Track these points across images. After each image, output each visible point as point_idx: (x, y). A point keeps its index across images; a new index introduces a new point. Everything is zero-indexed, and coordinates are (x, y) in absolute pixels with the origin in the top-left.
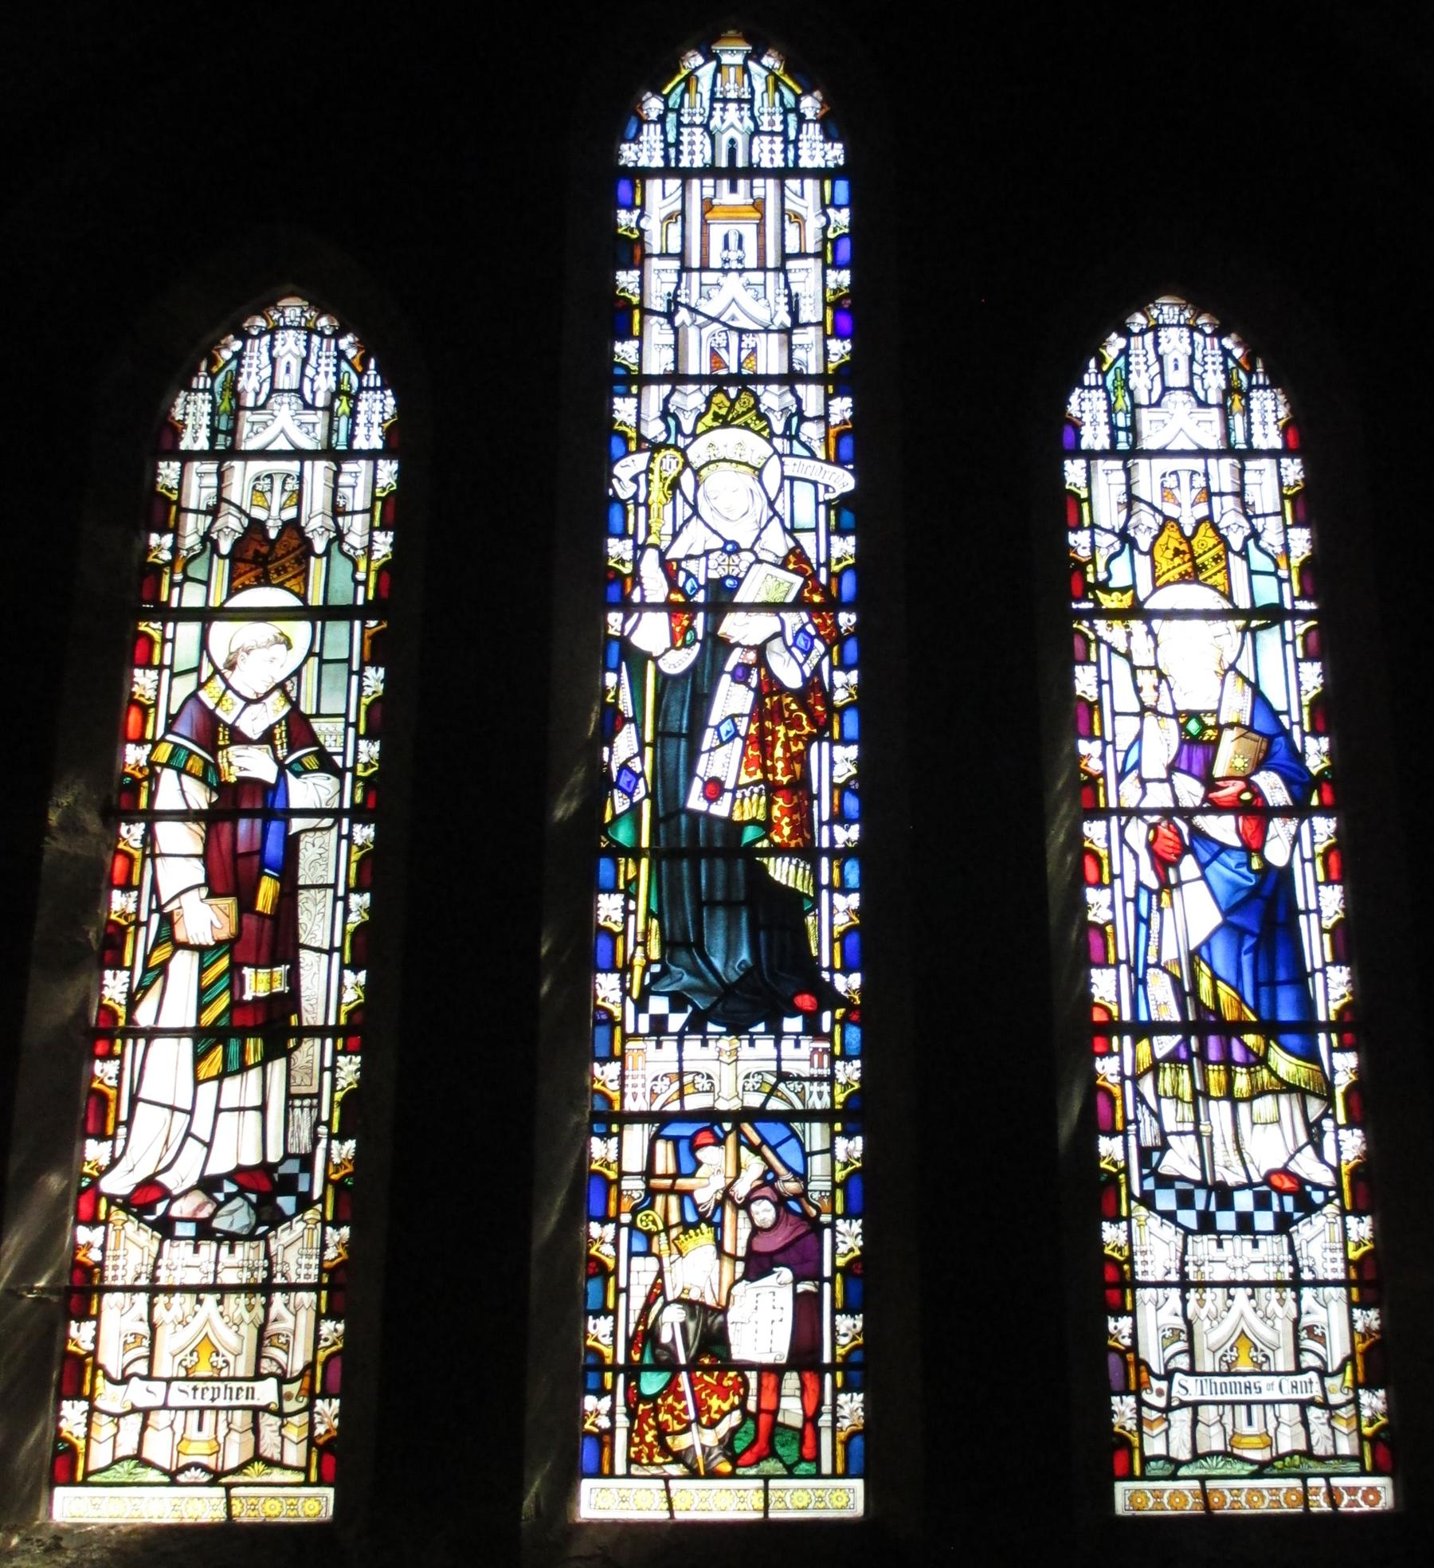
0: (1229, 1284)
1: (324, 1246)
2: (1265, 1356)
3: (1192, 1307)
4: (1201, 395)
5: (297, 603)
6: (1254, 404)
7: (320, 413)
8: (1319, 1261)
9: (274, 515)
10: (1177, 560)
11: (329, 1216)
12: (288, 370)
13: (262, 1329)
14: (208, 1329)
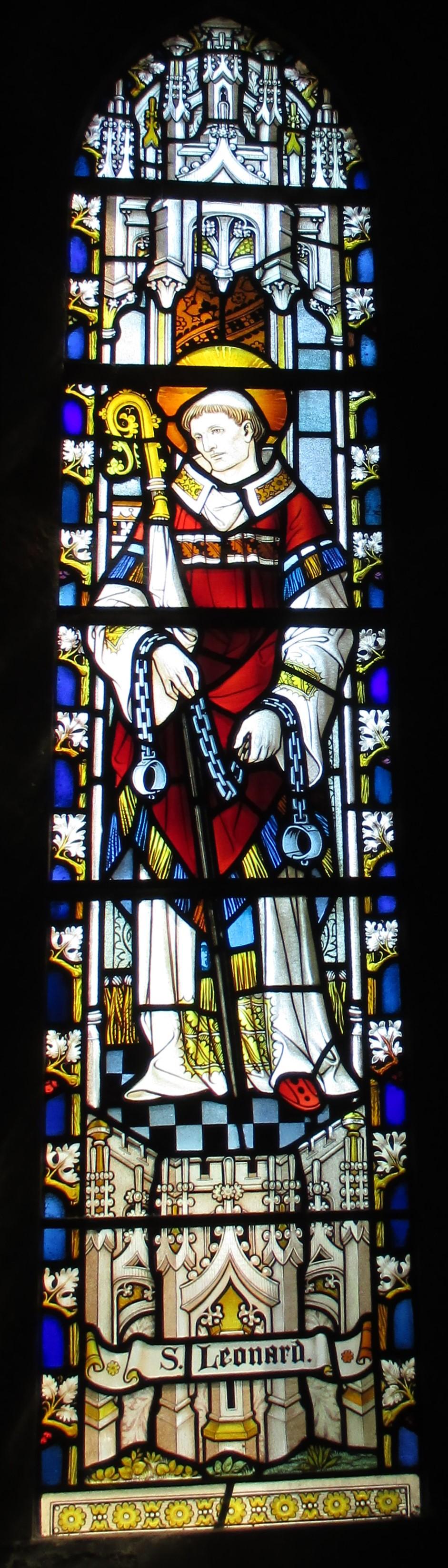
0: (211, 1221)
1: (373, 1161)
2: (258, 1315)
3: (162, 1254)
4: (251, 129)
5: (258, 363)
6: (317, 145)
7: (267, 149)
8: (335, 1186)
9: (225, 262)
10: (206, 317)
11: (375, 1120)
12: (224, 98)
13: (302, 1269)
14: (230, 1273)
